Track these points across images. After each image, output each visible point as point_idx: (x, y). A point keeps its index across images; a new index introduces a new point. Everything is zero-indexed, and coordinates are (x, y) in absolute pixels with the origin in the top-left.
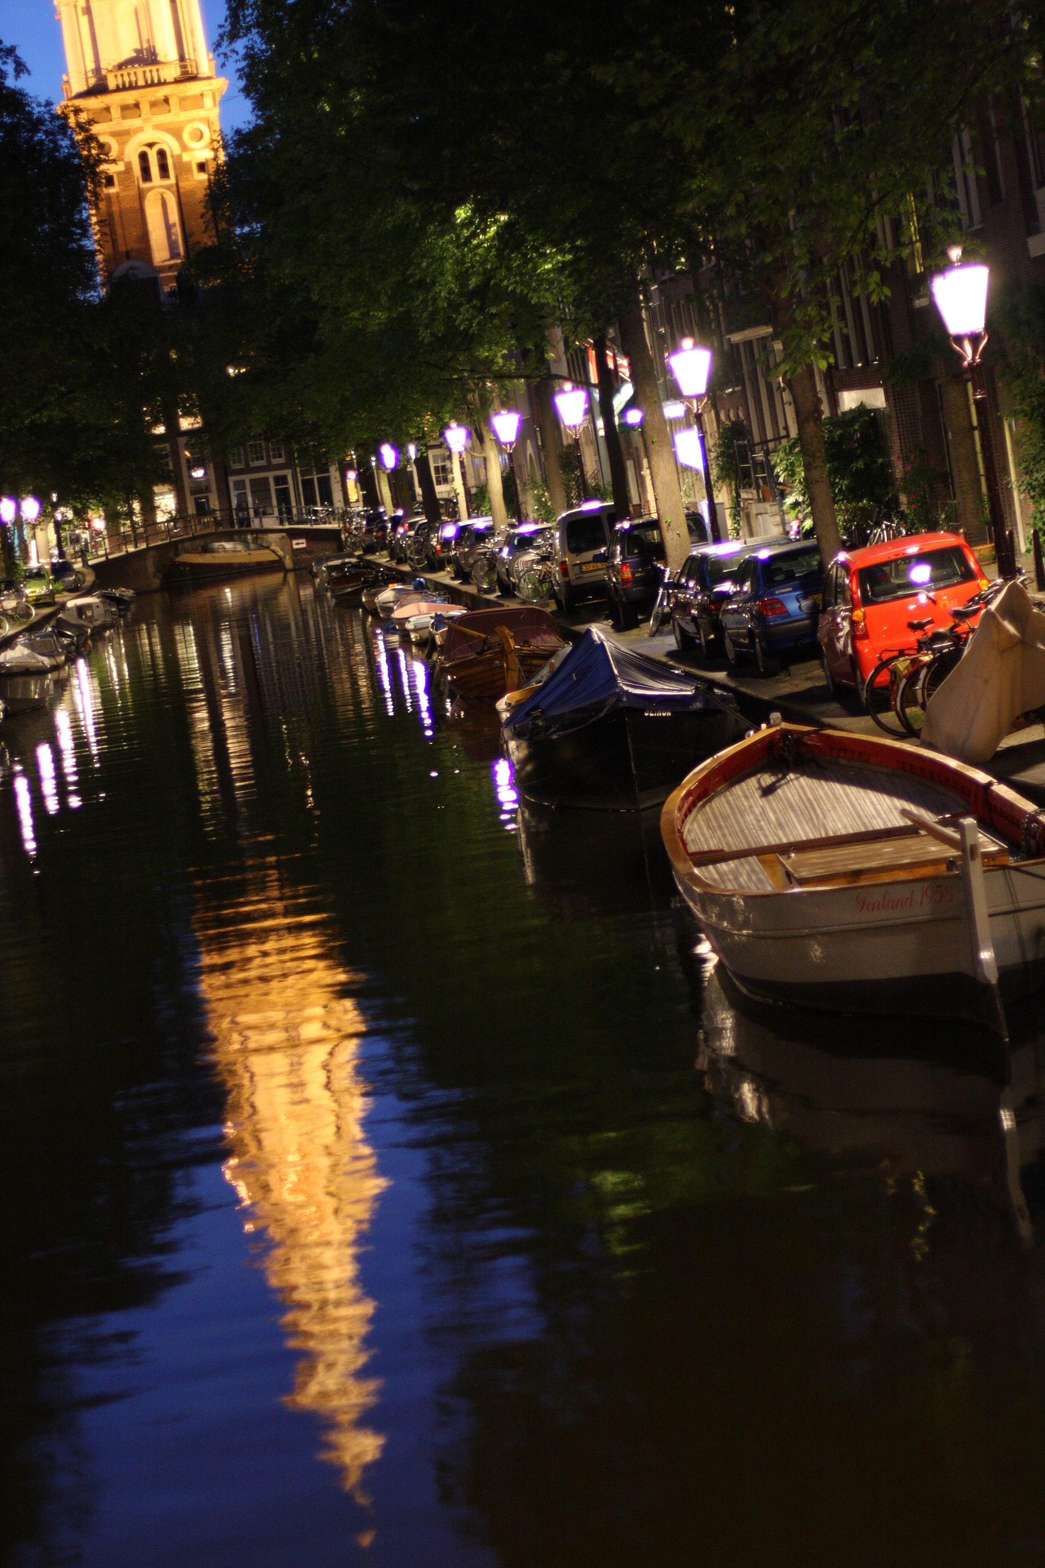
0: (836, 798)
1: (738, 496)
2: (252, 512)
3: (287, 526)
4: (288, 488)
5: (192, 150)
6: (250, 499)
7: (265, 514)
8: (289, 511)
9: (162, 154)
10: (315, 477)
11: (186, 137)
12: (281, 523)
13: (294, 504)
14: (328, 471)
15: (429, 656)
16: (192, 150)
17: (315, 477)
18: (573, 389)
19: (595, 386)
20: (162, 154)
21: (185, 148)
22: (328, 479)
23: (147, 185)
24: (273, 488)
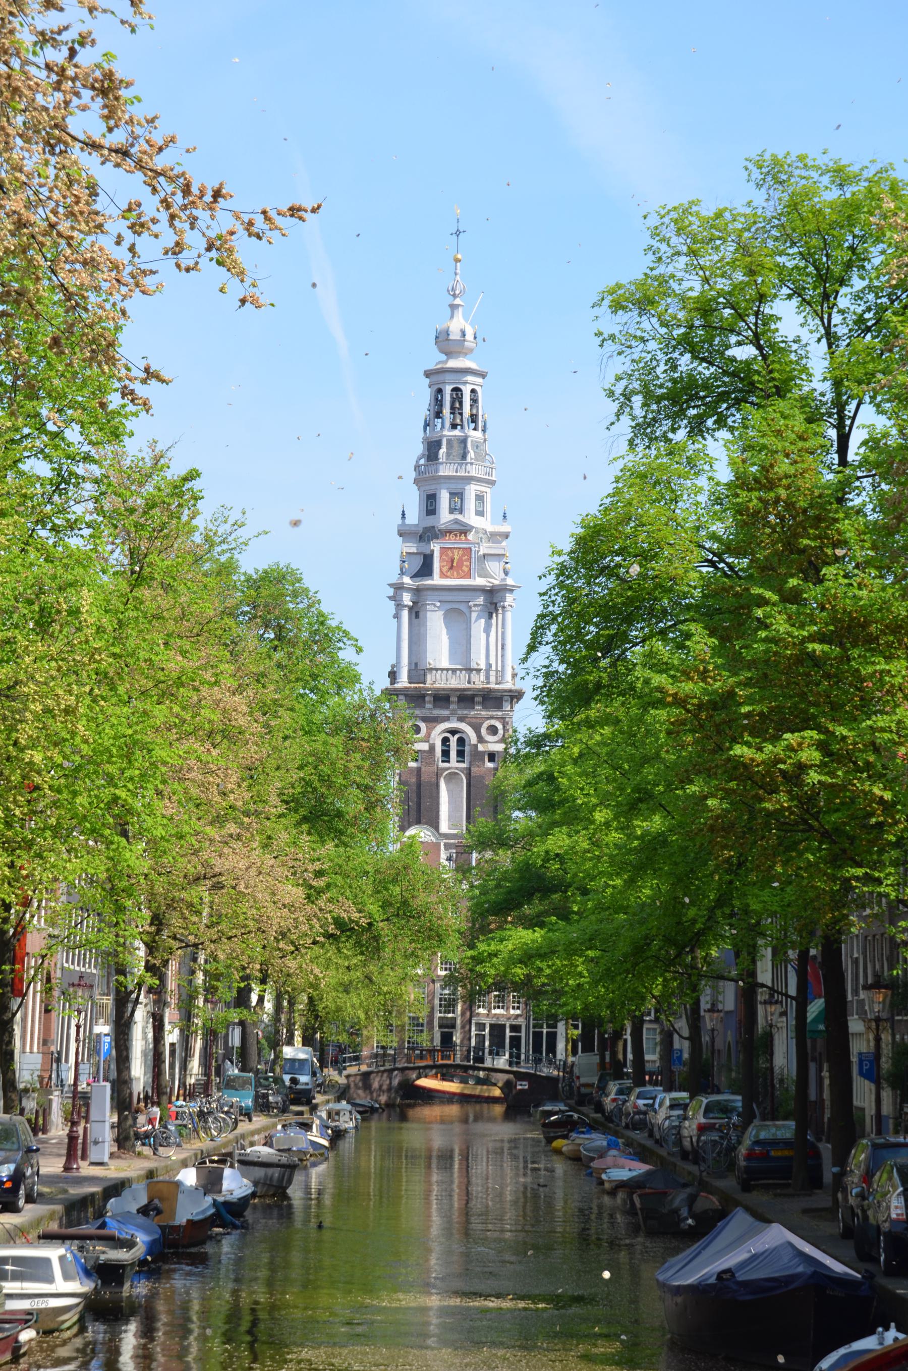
0: (381, 1197)
1: (901, 1109)
2: (487, 1051)
3: (515, 1069)
4: (520, 1037)
5: (487, 742)
6: (487, 1043)
7: (498, 1054)
8: (518, 1057)
9: (461, 742)
10: (545, 1031)
11: (483, 731)
12: (510, 1065)
13: (523, 1050)
14: (556, 1027)
15: (479, 993)
16: (487, 742)
17: (545, 1031)
18: (677, 1304)
19: (792, 998)
20: (461, 742)
21: (481, 739)
22: (555, 1034)
23: (446, 765)
24: (508, 1033)
